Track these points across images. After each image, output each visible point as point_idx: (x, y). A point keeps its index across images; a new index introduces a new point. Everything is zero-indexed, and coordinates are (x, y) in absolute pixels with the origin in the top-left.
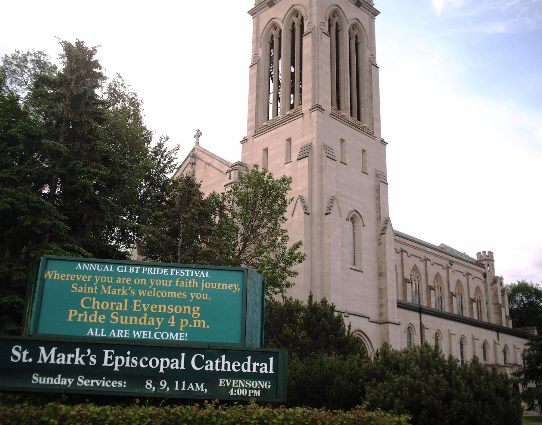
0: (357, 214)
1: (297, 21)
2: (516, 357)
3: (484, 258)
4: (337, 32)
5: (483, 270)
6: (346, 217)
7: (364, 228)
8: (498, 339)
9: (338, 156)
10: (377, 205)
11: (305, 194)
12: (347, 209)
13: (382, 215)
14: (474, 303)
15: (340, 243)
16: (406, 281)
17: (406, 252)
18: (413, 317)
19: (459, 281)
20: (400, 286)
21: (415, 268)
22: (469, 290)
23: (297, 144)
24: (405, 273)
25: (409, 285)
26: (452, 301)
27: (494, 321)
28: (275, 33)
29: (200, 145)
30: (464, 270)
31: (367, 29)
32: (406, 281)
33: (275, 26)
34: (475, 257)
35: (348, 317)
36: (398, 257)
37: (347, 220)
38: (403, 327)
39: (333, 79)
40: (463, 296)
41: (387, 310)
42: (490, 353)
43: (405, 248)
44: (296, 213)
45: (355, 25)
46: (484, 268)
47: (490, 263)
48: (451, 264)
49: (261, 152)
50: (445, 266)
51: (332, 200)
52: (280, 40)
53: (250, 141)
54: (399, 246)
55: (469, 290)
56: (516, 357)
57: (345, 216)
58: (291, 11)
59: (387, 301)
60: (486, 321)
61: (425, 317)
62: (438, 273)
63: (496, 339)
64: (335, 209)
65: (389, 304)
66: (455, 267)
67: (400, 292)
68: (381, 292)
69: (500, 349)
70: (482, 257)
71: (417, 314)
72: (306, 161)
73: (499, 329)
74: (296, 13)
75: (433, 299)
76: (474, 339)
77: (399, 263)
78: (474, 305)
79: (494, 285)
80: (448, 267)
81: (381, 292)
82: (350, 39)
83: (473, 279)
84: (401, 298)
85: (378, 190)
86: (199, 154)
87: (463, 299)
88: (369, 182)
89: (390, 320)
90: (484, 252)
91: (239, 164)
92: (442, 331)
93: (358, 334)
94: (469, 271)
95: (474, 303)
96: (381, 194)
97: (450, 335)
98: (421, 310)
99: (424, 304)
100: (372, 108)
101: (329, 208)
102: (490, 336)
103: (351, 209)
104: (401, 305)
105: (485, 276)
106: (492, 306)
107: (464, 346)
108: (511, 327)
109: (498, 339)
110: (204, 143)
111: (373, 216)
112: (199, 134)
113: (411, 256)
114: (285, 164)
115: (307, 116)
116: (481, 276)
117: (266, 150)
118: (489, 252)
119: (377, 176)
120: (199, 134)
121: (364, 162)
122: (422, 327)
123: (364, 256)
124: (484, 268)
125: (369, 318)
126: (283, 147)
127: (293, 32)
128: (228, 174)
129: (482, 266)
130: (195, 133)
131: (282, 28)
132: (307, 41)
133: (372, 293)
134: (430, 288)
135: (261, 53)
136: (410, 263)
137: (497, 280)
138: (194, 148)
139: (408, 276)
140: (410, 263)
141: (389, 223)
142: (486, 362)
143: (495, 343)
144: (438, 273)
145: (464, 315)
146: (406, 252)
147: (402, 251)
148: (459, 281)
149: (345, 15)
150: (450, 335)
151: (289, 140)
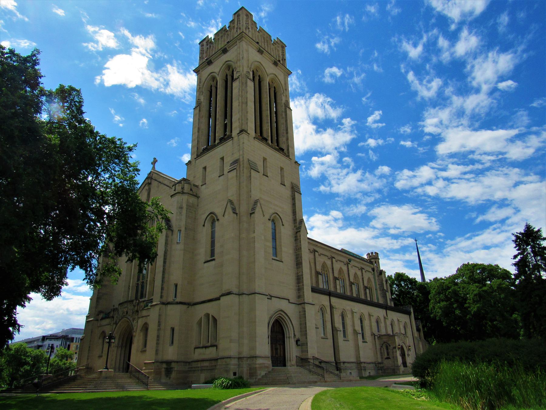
0: (278, 216)
1: (229, 73)
2: (400, 329)
3: (372, 257)
4: (260, 82)
5: (372, 266)
6: (268, 217)
7: (283, 227)
8: (387, 315)
9: (261, 169)
10: (293, 210)
11: (234, 198)
12: (269, 212)
13: (297, 217)
14: (367, 290)
15: (263, 238)
16: (318, 273)
17: (317, 252)
18: (324, 300)
19: (356, 274)
20: (314, 277)
21: (324, 265)
22: (363, 280)
23: (228, 160)
24: (317, 267)
25: (320, 277)
26: (352, 287)
27: (381, 301)
28: (213, 84)
29: (156, 169)
30: (359, 266)
31: (283, 82)
32: (318, 273)
33: (214, 78)
34: (365, 257)
35: (271, 299)
36: (312, 256)
37: (269, 220)
38: (317, 307)
39: (257, 114)
40: (359, 285)
41: (304, 292)
42: (382, 325)
43: (317, 249)
44: (226, 213)
45: (273, 79)
46: (373, 264)
47: (377, 261)
48: (350, 262)
49: (201, 170)
50: (345, 262)
51: (256, 202)
52: (216, 88)
53: (193, 163)
54: (312, 247)
55: (363, 280)
56: (400, 329)
57: (267, 216)
58: (224, 66)
59: (303, 285)
60: (376, 301)
61: (333, 300)
62: (341, 268)
63: (385, 315)
64: (258, 209)
65: (305, 287)
66: (352, 263)
67: (314, 281)
68: (299, 279)
69: (388, 323)
70: (370, 256)
71: (327, 297)
72: (234, 173)
73: (386, 307)
74: (229, 67)
75: (338, 287)
76: (370, 315)
77: (312, 261)
78: (368, 291)
79: (380, 276)
80: (348, 264)
81: (299, 279)
82: (269, 89)
83: (365, 272)
84: (314, 285)
85: (294, 199)
86: (154, 176)
87: (359, 286)
88: (286, 192)
89: (306, 301)
90: (372, 253)
91: (184, 179)
92: (346, 310)
93: (280, 314)
94: (363, 266)
95: (367, 290)
96: (296, 201)
97: (353, 313)
98: (330, 294)
99: (332, 289)
100: (287, 139)
101: (253, 209)
102: (380, 313)
103: (273, 211)
104: (314, 290)
105: (373, 270)
106: (379, 292)
107: (363, 322)
108: (393, 305)
109: (387, 315)
110: (158, 168)
111: (291, 217)
112: (155, 162)
113: (321, 255)
114: (219, 177)
115: (236, 138)
116: (371, 270)
117: (205, 168)
118: (375, 253)
119: (292, 188)
120: (155, 162)
121: (282, 177)
122: (331, 307)
123: (284, 249)
124: (373, 264)
125: (289, 300)
126: (218, 163)
127: (226, 82)
128: (174, 187)
129: (371, 263)
130: (152, 160)
131: (218, 79)
132: (236, 84)
133: (291, 280)
134: (335, 279)
135: (202, 98)
136: (320, 260)
137: (381, 272)
138: (151, 172)
139: (319, 269)
140: (320, 260)
141: (303, 223)
142: (379, 333)
143: (385, 318)
144: (341, 268)
145: (361, 297)
146: (317, 252)
147: (315, 251)
148: (356, 274)
149: (265, 70)
150: (353, 313)
151: (222, 159)
